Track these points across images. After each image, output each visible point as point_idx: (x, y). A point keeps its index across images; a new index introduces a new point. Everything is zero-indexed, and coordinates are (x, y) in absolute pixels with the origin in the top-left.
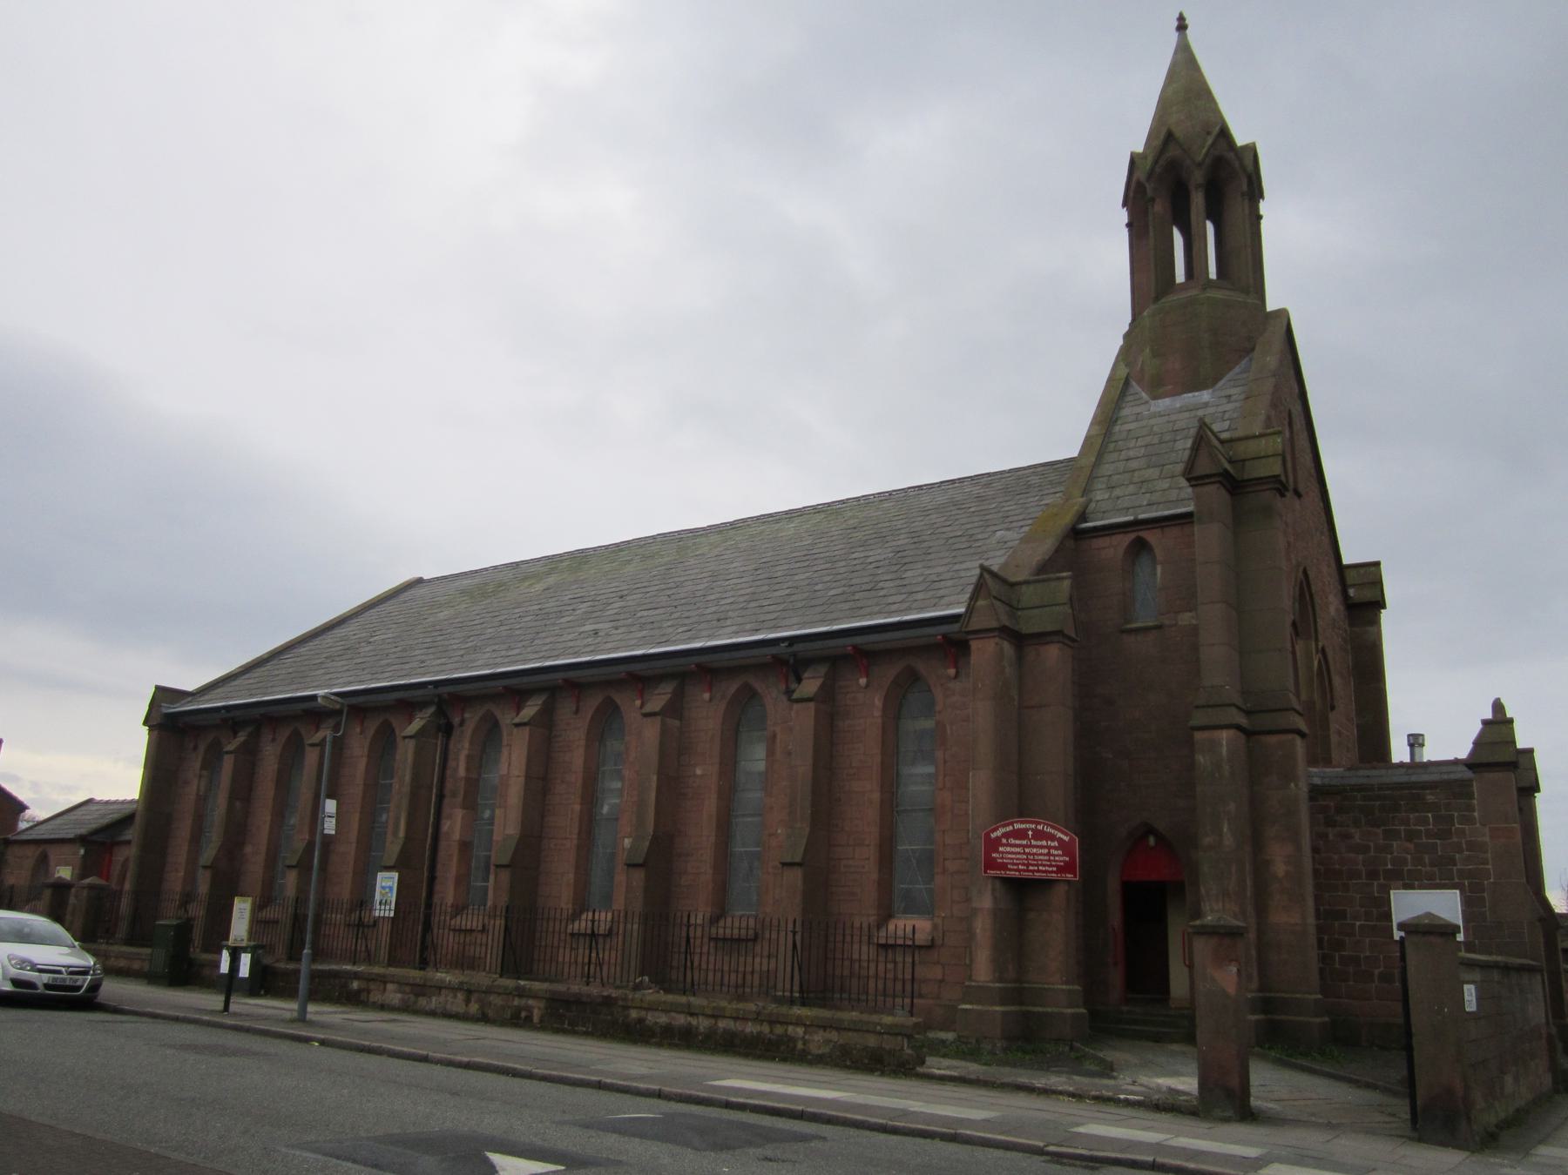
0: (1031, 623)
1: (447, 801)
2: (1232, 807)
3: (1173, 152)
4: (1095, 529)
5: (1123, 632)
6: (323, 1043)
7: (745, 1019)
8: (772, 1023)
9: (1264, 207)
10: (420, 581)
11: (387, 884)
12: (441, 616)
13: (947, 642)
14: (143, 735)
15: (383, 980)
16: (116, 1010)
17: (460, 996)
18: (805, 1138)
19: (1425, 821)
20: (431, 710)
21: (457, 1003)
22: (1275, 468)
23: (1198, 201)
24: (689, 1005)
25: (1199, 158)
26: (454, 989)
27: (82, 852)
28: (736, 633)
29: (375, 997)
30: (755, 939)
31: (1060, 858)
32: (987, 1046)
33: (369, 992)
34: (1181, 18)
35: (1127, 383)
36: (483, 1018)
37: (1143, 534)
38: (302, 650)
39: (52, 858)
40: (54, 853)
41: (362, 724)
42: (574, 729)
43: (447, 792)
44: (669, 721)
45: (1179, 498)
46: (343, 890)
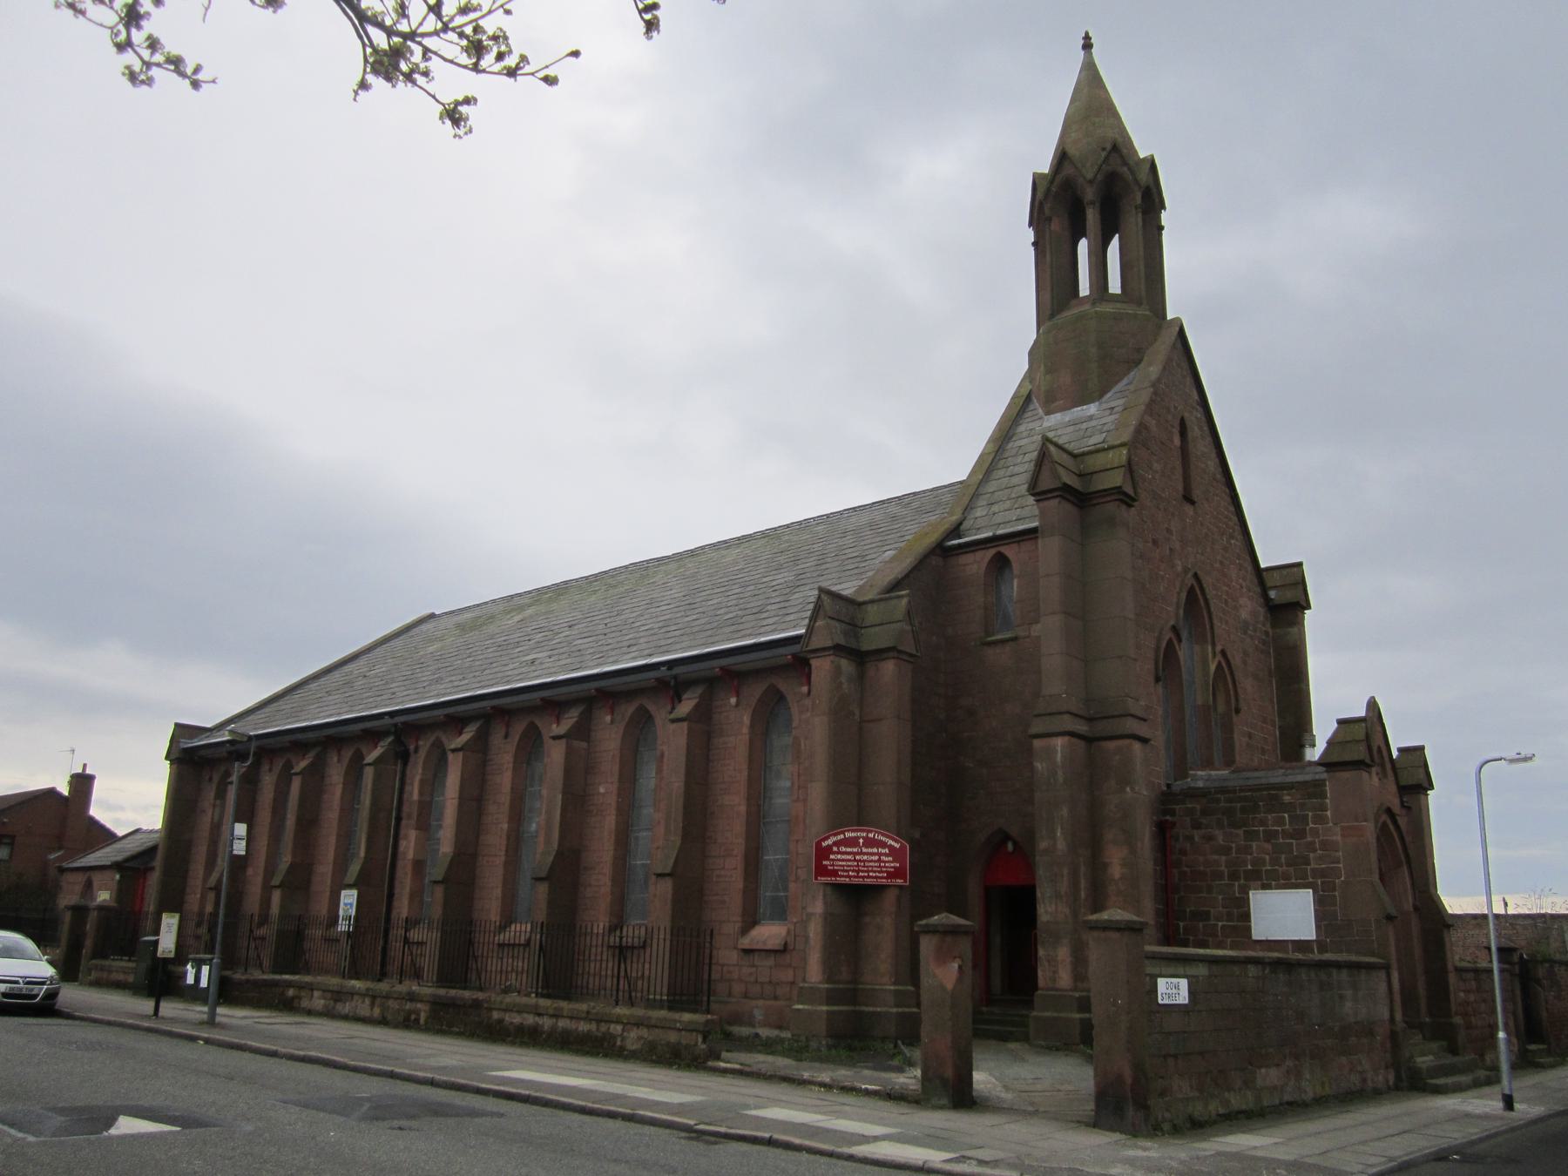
0: (873, 639)
1: (404, 822)
2: (1065, 812)
3: (1068, 170)
4: (960, 546)
5: (990, 644)
6: (207, 1041)
7: (579, 1019)
8: (599, 1021)
9: (1165, 217)
10: (432, 616)
11: (349, 899)
12: (431, 649)
13: (786, 663)
14: (165, 769)
15: (311, 988)
16: (69, 1016)
17: (367, 1001)
18: (473, 1113)
19: (1281, 822)
20: (390, 739)
21: (364, 1008)
22: (1116, 479)
23: (1092, 217)
24: (537, 1006)
25: (1090, 176)
26: (363, 995)
27: (118, 877)
28: (634, 659)
29: (305, 1003)
30: (644, 947)
31: (891, 864)
32: (814, 1044)
33: (300, 998)
34: (1087, 37)
35: (1028, 399)
36: (383, 1022)
37: (1003, 549)
38: (313, 686)
39: (96, 884)
40: (97, 878)
41: (339, 751)
42: (504, 753)
43: (404, 815)
44: (576, 744)
45: (1026, 515)
46: (321, 908)
